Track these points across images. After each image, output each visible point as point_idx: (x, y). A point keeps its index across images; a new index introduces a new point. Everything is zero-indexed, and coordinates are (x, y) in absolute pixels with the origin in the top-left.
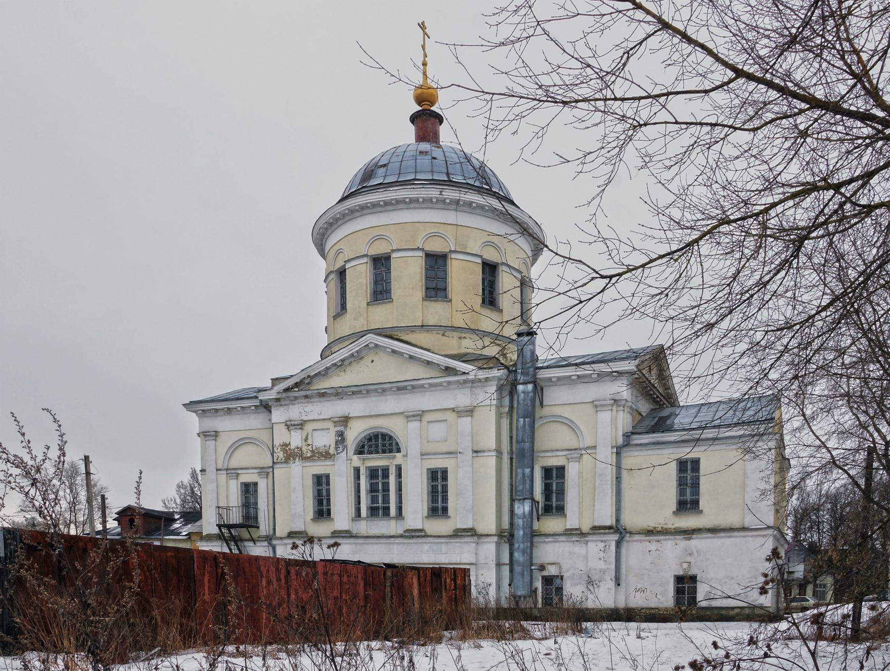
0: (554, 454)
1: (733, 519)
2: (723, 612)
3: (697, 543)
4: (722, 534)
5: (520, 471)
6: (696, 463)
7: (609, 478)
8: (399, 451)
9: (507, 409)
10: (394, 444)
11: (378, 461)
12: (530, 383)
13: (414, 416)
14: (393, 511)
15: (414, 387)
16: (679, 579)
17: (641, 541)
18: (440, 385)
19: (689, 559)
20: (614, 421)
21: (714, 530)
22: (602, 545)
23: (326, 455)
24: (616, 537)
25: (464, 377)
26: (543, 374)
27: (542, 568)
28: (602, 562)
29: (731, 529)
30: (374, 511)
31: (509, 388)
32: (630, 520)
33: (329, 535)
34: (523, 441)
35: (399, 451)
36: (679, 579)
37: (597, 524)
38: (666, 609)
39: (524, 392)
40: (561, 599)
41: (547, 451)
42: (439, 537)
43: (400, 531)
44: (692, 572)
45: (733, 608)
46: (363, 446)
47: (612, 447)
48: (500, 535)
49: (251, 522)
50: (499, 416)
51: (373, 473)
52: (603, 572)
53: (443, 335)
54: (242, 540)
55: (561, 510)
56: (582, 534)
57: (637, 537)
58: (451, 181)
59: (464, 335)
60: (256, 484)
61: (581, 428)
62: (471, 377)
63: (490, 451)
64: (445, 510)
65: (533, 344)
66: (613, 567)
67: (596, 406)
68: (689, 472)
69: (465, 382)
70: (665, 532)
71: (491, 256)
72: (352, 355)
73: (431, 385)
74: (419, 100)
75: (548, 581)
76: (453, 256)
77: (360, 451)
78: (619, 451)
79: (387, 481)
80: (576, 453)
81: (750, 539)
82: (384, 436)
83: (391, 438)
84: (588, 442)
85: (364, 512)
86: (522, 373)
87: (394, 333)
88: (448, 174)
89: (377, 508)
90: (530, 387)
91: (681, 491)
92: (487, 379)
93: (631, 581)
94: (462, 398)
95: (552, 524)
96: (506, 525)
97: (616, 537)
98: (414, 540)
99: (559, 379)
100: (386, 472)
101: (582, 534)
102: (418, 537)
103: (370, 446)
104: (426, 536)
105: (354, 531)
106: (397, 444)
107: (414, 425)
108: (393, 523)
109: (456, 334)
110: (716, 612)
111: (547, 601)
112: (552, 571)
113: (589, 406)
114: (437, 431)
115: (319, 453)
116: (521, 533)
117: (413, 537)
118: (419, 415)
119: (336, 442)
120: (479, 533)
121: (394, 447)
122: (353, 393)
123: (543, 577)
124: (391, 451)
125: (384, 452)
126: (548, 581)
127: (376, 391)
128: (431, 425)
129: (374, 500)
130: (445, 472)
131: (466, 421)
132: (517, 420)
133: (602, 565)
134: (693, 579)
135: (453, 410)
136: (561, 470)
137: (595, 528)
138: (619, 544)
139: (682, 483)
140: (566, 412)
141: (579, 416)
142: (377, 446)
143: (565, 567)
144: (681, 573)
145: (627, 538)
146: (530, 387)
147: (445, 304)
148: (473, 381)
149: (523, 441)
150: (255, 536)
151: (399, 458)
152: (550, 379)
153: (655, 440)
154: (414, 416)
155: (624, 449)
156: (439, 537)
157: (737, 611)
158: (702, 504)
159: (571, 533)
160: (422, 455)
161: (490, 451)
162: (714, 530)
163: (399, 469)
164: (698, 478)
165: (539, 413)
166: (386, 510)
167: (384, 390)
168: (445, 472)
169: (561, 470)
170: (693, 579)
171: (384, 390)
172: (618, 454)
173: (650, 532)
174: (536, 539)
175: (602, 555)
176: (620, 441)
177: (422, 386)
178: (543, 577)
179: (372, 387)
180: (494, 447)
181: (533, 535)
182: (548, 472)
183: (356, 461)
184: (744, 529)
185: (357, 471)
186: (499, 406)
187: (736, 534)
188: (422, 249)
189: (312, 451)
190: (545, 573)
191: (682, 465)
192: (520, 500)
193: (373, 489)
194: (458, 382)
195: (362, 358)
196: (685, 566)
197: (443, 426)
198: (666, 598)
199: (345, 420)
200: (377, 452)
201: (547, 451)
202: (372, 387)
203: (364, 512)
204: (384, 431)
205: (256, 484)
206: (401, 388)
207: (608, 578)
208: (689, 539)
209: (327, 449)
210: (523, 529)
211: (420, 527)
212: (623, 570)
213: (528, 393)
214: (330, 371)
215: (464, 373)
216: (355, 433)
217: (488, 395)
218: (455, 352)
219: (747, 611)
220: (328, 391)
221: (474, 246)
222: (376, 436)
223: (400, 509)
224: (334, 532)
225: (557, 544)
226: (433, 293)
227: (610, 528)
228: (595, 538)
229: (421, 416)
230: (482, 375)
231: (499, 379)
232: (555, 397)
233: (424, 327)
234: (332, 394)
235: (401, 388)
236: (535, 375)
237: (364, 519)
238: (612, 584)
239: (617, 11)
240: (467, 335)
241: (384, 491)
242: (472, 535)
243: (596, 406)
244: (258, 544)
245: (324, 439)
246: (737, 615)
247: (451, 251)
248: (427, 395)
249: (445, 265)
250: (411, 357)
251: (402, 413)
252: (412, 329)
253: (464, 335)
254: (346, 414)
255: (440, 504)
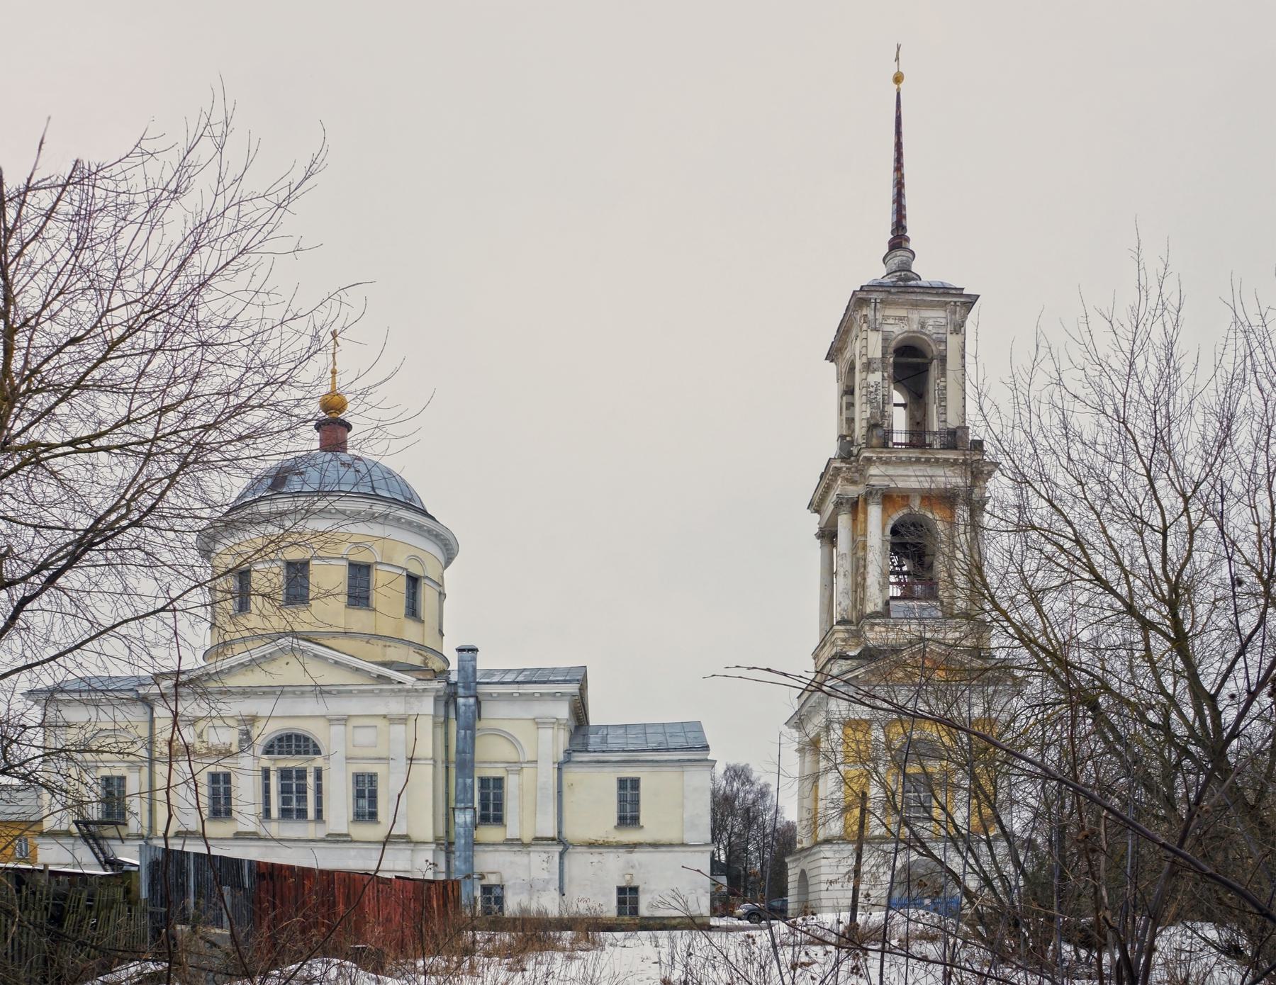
0: (492, 765)
1: (672, 835)
2: (666, 922)
3: (638, 857)
4: (664, 849)
5: (460, 780)
6: (635, 783)
7: (551, 792)
8: (318, 752)
9: (442, 719)
10: (311, 746)
11: (293, 762)
12: (471, 696)
13: (338, 720)
14: (311, 813)
15: (339, 692)
16: (621, 890)
17: (582, 853)
18: (372, 691)
19: (631, 871)
20: (555, 739)
21: (655, 845)
22: (545, 856)
23: (228, 754)
24: (560, 848)
25: (400, 686)
26: (483, 689)
27: (482, 877)
28: (545, 872)
29: (671, 845)
30: (286, 813)
31: (449, 699)
32: (571, 833)
33: (231, 836)
34: (465, 752)
35: (318, 752)
36: (621, 890)
37: (539, 835)
38: (610, 919)
39: (465, 705)
40: (501, 909)
41: (485, 762)
42: (369, 842)
43: (321, 835)
44: (634, 884)
45: (674, 918)
46: (272, 746)
47: (554, 763)
48: (437, 841)
49: (116, 819)
50: (435, 724)
51: (285, 774)
52: (547, 882)
53: (368, 642)
54: (104, 838)
55: (499, 820)
56: (523, 845)
57: (579, 849)
58: (378, 495)
59: (388, 644)
60: (123, 779)
61: (522, 743)
62: (408, 686)
63: (426, 759)
64: (229, 813)
65: (474, 659)
66: (557, 877)
67: (537, 723)
68: (629, 789)
69: (400, 691)
70: (606, 845)
71: (416, 570)
72: (264, 656)
73: (360, 691)
74: (326, 407)
75: (487, 889)
76: (379, 567)
77: (269, 750)
78: (559, 769)
79: (302, 782)
80: (516, 766)
81: (689, 854)
82: (298, 737)
83: (307, 739)
84: (529, 757)
85: (275, 813)
86: (464, 687)
87: (312, 637)
88: (373, 489)
89: (290, 811)
90: (472, 700)
91: (621, 808)
92: (424, 690)
93: (573, 892)
94: (395, 706)
95: (489, 833)
96: (441, 833)
97: (560, 848)
98: (340, 845)
99: (499, 694)
100: (302, 774)
101: (523, 845)
102: (345, 841)
103: (280, 747)
104: (351, 841)
105: (263, 833)
106: (315, 745)
107: (337, 729)
108: (311, 826)
109: (381, 643)
110: (658, 921)
111: (487, 911)
112: (492, 880)
113: (530, 723)
114: (364, 737)
115: (216, 750)
116: (463, 841)
117: (338, 842)
118: (344, 720)
119: (240, 741)
120: (414, 840)
121: (311, 749)
122: (264, 693)
123: (482, 886)
124: (307, 753)
125: (298, 753)
126: (487, 889)
127: (294, 693)
128: (358, 730)
129: (286, 801)
130: (372, 778)
131: (399, 729)
132: (458, 732)
133: (545, 875)
134: (635, 890)
135: (385, 717)
136: (499, 782)
137: (537, 839)
138: (562, 855)
139: (622, 800)
140: (507, 727)
141: (522, 731)
142: (290, 746)
143: (506, 876)
144: (623, 884)
145: (570, 850)
146: (472, 700)
147: (370, 613)
148: (408, 691)
149: (465, 752)
150: (123, 834)
151: (319, 761)
152: (491, 694)
153: (595, 759)
154: (338, 720)
155: (566, 765)
156: (369, 842)
157: (678, 920)
158: (642, 821)
159: (510, 843)
160: (347, 759)
161: (426, 759)
162: (655, 845)
163: (319, 774)
164: (638, 795)
165: (479, 725)
166: (302, 814)
167: (303, 693)
168: (372, 778)
169: (499, 782)
170: (635, 890)
171: (303, 693)
172: (559, 769)
173: (591, 845)
174: (476, 848)
175: (545, 865)
176: (561, 757)
177: (351, 692)
178: (482, 886)
179: (290, 689)
180: (431, 755)
181: (473, 844)
182: (484, 782)
183: (266, 761)
184: (683, 845)
185: (266, 773)
186: (435, 716)
187: (676, 849)
188: (347, 559)
189: (208, 748)
190: (484, 882)
191: (622, 783)
192: (461, 809)
193: (285, 790)
194: (392, 690)
195: (274, 660)
196: (628, 877)
197: (371, 732)
198: (610, 909)
199: (253, 719)
200: (289, 753)
201: (485, 762)
202: (290, 689)
203: (275, 813)
204: (300, 732)
205: (123, 779)
206: (321, 692)
207: (552, 888)
208: (631, 852)
209: (227, 746)
210: (466, 837)
211: (345, 831)
212: (566, 880)
213: (470, 706)
214: (234, 670)
215: (400, 683)
216: (266, 732)
217: (427, 706)
218: (379, 660)
219: (687, 921)
220: (233, 690)
221: (401, 560)
222: (289, 737)
223: (319, 813)
224: (237, 834)
225: (497, 854)
226: (353, 601)
227: (553, 839)
228: (539, 848)
229: (346, 720)
230: (420, 685)
231: (438, 691)
232: (495, 713)
233: (347, 634)
234: (238, 693)
235: (321, 692)
236: (475, 689)
237: (274, 821)
238: (556, 894)
239: (64, 187)
240: (391, 644)
241: (298, 792)
242: (408, 842)
243: (537, 723)
244: (127, 843)
245: (228, 737)
246: (679, 924)
247: (376, 563)
248: (354, 700)
249: (368, 575)
250: (336, 662)
251: (324, 716)
252: (334, 635)
253: (388, 644)
254: (254, 713)
255: (294, 805)
